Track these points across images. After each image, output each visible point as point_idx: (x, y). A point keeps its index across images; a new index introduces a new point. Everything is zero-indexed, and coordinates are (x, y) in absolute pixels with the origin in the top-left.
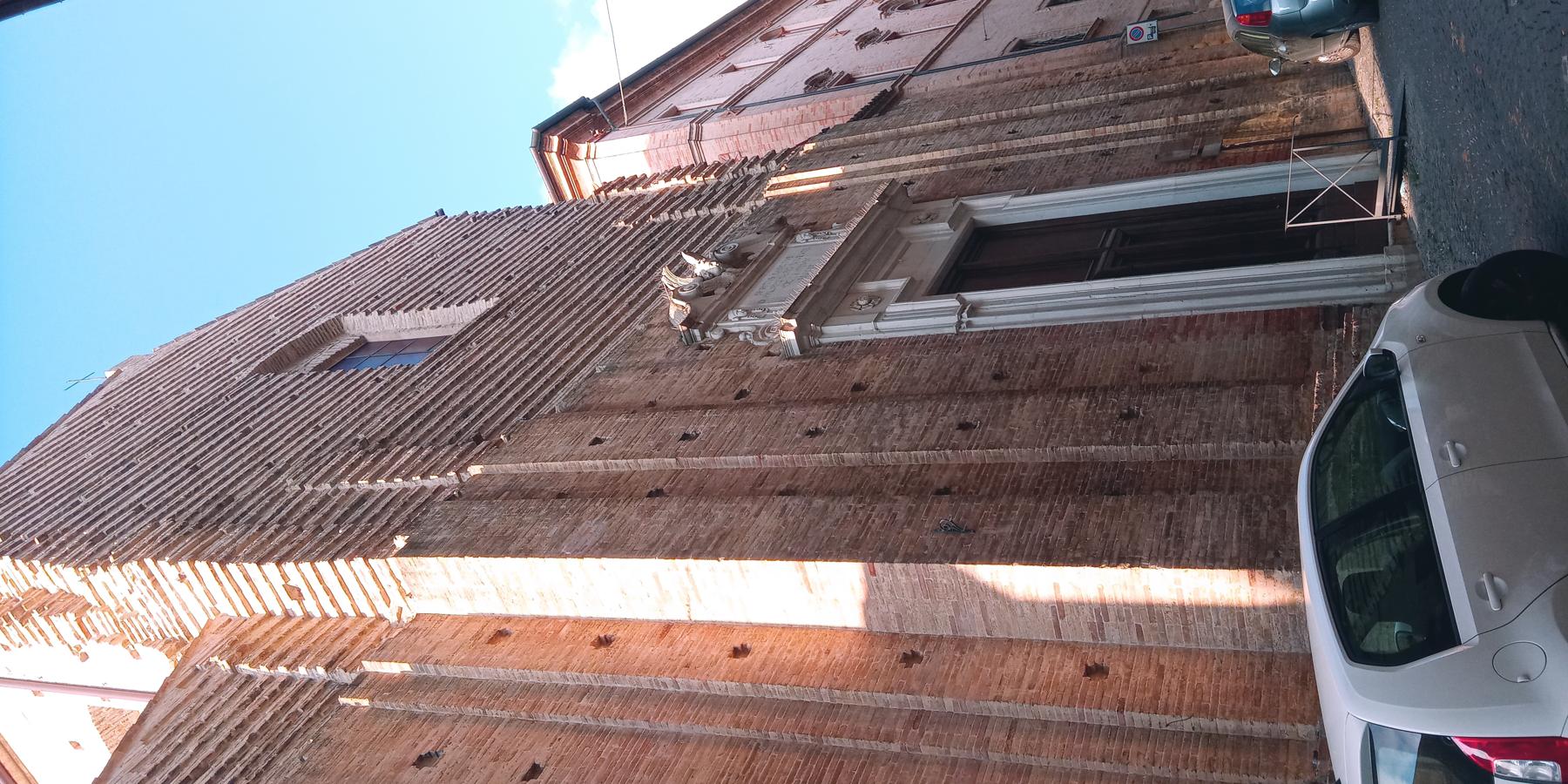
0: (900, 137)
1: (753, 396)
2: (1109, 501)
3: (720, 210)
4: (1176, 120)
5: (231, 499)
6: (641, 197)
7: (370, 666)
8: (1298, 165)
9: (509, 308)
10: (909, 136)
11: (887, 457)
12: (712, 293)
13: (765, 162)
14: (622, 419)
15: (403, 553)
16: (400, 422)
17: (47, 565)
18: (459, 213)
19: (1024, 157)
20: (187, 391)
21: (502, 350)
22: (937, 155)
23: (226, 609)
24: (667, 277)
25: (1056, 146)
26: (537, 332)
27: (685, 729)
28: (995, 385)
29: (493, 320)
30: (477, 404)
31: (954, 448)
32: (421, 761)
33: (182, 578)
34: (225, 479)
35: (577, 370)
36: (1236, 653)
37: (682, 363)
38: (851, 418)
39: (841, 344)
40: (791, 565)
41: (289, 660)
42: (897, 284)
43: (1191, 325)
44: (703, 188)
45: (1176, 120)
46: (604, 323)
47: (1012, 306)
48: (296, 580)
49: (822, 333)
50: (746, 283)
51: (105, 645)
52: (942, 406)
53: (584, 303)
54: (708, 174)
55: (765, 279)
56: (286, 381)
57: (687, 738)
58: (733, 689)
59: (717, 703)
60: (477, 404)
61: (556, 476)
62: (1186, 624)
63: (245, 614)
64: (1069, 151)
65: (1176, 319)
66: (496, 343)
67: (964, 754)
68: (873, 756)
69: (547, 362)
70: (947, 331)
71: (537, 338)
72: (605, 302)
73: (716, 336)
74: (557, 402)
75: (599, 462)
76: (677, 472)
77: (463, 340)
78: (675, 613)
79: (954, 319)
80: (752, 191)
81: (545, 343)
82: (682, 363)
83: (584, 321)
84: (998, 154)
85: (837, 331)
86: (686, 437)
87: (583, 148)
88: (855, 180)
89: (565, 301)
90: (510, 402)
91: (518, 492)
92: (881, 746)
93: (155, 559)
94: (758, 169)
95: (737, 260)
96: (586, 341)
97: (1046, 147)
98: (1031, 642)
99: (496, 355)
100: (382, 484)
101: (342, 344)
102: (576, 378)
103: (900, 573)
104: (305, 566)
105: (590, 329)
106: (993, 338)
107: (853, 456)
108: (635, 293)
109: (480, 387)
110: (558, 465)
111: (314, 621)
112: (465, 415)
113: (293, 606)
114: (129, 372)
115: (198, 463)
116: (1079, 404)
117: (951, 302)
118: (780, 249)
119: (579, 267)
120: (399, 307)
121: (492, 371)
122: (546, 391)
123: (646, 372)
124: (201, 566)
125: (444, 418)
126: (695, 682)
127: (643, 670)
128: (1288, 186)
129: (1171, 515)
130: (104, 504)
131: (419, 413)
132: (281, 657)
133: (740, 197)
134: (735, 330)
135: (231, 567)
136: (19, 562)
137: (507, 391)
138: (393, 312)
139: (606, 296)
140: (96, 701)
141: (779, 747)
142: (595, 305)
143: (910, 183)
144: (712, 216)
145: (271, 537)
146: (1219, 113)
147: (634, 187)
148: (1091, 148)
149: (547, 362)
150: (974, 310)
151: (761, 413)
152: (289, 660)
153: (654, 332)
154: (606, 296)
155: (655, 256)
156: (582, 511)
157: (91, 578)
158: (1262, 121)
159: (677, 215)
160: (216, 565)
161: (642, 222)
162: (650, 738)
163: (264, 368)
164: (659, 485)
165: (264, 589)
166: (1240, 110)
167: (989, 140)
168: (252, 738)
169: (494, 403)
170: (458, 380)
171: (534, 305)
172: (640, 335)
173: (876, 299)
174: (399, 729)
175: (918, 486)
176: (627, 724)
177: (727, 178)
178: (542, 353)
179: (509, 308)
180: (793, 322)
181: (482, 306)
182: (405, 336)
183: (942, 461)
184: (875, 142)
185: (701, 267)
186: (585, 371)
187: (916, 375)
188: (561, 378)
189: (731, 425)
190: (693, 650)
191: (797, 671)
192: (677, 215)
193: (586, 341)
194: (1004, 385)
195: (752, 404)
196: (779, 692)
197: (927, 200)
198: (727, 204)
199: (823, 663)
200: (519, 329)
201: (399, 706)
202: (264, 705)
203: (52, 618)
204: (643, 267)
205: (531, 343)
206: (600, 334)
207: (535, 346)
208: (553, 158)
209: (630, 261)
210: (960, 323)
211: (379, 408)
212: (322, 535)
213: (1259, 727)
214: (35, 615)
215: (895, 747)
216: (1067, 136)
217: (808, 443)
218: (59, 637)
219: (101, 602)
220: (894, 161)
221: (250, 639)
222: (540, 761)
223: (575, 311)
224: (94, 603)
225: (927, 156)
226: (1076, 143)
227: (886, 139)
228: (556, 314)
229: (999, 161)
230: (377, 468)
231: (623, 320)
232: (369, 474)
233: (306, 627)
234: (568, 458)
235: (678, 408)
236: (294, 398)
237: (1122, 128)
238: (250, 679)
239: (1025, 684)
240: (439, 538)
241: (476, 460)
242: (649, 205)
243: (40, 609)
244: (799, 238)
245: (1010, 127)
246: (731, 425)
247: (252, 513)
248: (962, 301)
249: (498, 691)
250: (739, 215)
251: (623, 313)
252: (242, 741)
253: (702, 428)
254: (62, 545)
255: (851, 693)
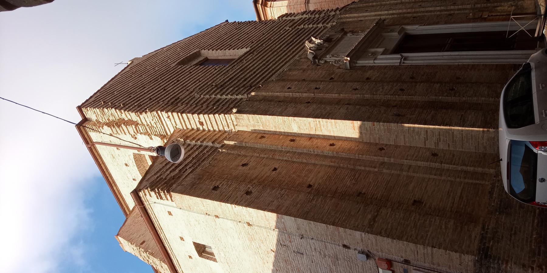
0: (381, 5)
1: (335, 79)
2: (445, 111)
3: (320, 25)
4: (474, 6)
5: (179, 98)
6: (293, 20)
7: (226, 142)
8: (513, 23)
9: (254, 51)
10: (385, 5)
11: (378, 97)
12: (321, 49)
13: (335, 11)
14: (296, 83)
15: (235, 113)
16: (226, 81)
17: (126, 112)
18: (233, 21)
19: (423, 14)
20: (157, 69)
21: (254, 63)
22: (394, 12)
23: (179, 126)
24: (307, 44)
25: (434, 11)
26: (264, 58)
27: (316, 162)
28: (411, 80)
29: (250, 54)
30: (248, 78)
31: (398, 95)
32: (243, 165)
33: (169, 117)
34: (175, 93)
35: (278, 70)
36: (476, 152)
37: (312, 69)
38: (367, 86)
39: (362, 66)
40: (350, 121)
41: (201, 140)
42: (381, 50)
43: (473, 67)
44: (314, 18)
45: (474, 6)
46: (285, 57)
47: (417, 58)
48: (202, 120)
49: (357, 63)
50: (331, 47)
51: (143, 135)
52: (395, 84)
53: (278, 51)
54: (316, 14)
55: (338, 46)
56: (187, 68)
57: (317, 165)
58: (330, 154)
59: (325, 157)
60: (248, 78)
61: (277, 97)
62: (462, 144)
63: (185, 128)
64: (438, 13)
65: (469, 65)
66: (251, 61)
67: (395, 172)
68: (369, 172)
69: (268, 67)
70: (396, 64)
71: (264, 60)
72: (285, 51)
73: (322, 62)
74: (273, 78)
75: (291, 94)
76: (314, 98)
77: (241, 59)
78: (313, 132)
79: (399, 61)
80: (331, 20)
81: (267, 62)
82: (312, 69)
83: (279, 56)
84: (415, 12)
85: (361, 62)
86: (316, 88)
87: (269, 3)
88: (366, 18)
89: (272, 50)
90: (258, 78)
91: (265, 100)
92: (372, 169)
93: (161, 111)
94: (333, 13)
95: (328, 40)
96: (280, 62)
97: (431, 11)
98: (417, 147)
99: (252, 64)
100: (224, 97)
101: (201, 59)
102: (278, 72)
103: (380, 127)
104: (206, 116)
105: (281, 59)
106: (411, 67)
107: (367, 96)
108: (294, 49)
109: (248, 73)
110: (278, 94)
111: (206, 132)
112: (245, 80)
113: (199, 126)
114: (136, 62)
115: (166, 88)
116: (437, 86)
117: (398, 56)
118: (342, 38)
119: (275, 40)
120: (218, 49)
121: (252, 68)
122: (269, 75)
123: (301, 71)
124: (175, 114)
125: (239, 81)
126: (319, 151)
127: (305, 147)
128: (508, 29)
129: (462, 115)
130: (139, 97)
131: (231, 79)
132: (198, 140)
133: (327, 21)
134: (329, 61)
135: (184, 115)
136: (117, 110)
137: (257, 74)
138: (217, 50)
139: (285, 49)
140: (136, 152)
141: (343, 168)
142: (282, 52)
143: (385, 20)
144: (317, 27)
145: (194, 108)
146: (489, 5)
147: (291, 17)
148: (445, 13)
149: (268, 67)
150: (406, 59)
151: (339, 83)
152: (201, 140)
153: (303, 60)
154: (285, 49)
155: (300, 38)
156: (287, 106)
157: (103, 131)
158: (502, 8)
159: (306, 26)
160: (179, 114)
161: (295, 27)
162: (307, 164)
163: (179, 64)
164: (309, 101)
165: (193, 121)
166: (496, 4)
167: (412, 8)
168: (193, 158)
169: (254, 77)
170: (241, 71)
171: (262, 51)
172: (299, 61)
173: (374, 54)
174: (236, 158)
175: (387, 105)
176: (300, 160)
177: (322, 15)
178: (267, 64)
179: (254, 51)
180: (349, 59)
181: (244, 50)
182: (220, 58)
183: (394, 99)
184: (373, 6)
185: (318, 41)
186: (281, 70)
187: (386, 76)
188: (273, 72)
189: (330, 86)
190: (319, 144)
191: (349, 150)
192: (306, 26)
193: (280, 62)
194: (331, 142)
195: (335, 81)
196: (344, 155)
197: (391, 25)
198: (323, 23)
199: (356, 148)
200: (258, 57)
201: (235, 152)
202: (195, 151)
203: (128, 126)
204: (296, 41)
205: (262, 62)
206: (284, 60)
207: (264, 62)
208: (259, 6)
209: (292, 39)
210: (400, 62)
211: (218, 77)
212: (209, 108)
213: (480, 170)
214: (123, 125)
215: (376, 170)
216: (438, 8)
217: (354, 92)
218: (129, 132)
219: (142, 123)
220: (380, 13)
221: (189, 134)
222: (277, 167)
223: (275, 53)
224: (140, 123)
225: (391, 12)
226: (441, 11)
227: (377, 6)
228: (269, 54)
229: (415, 15)
230: (222, 92)
231: (291, 56)
232: (220, 94)
233: (204, 133)
234: (281, 92)
235: (313, 81)
236: (191, 73)
237: (456, 7)
238: (189, 145)
239: (415, 156)
240: (246, 110)
241: (253, 91)
242: (297, 22)
243: (124, 124)
244: (348, 35)
245: (419, 4)
246: (330, 86)
247: (187, 102)
248: (402, 56)
249: (263, 150)
250: (327, 27)
251: (291, 55)
252: (191, 159)
253: (321, 87)
254: (129, 107)
255: (364, 156)
